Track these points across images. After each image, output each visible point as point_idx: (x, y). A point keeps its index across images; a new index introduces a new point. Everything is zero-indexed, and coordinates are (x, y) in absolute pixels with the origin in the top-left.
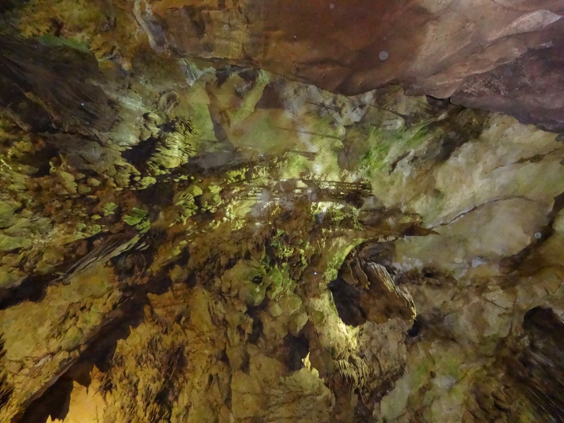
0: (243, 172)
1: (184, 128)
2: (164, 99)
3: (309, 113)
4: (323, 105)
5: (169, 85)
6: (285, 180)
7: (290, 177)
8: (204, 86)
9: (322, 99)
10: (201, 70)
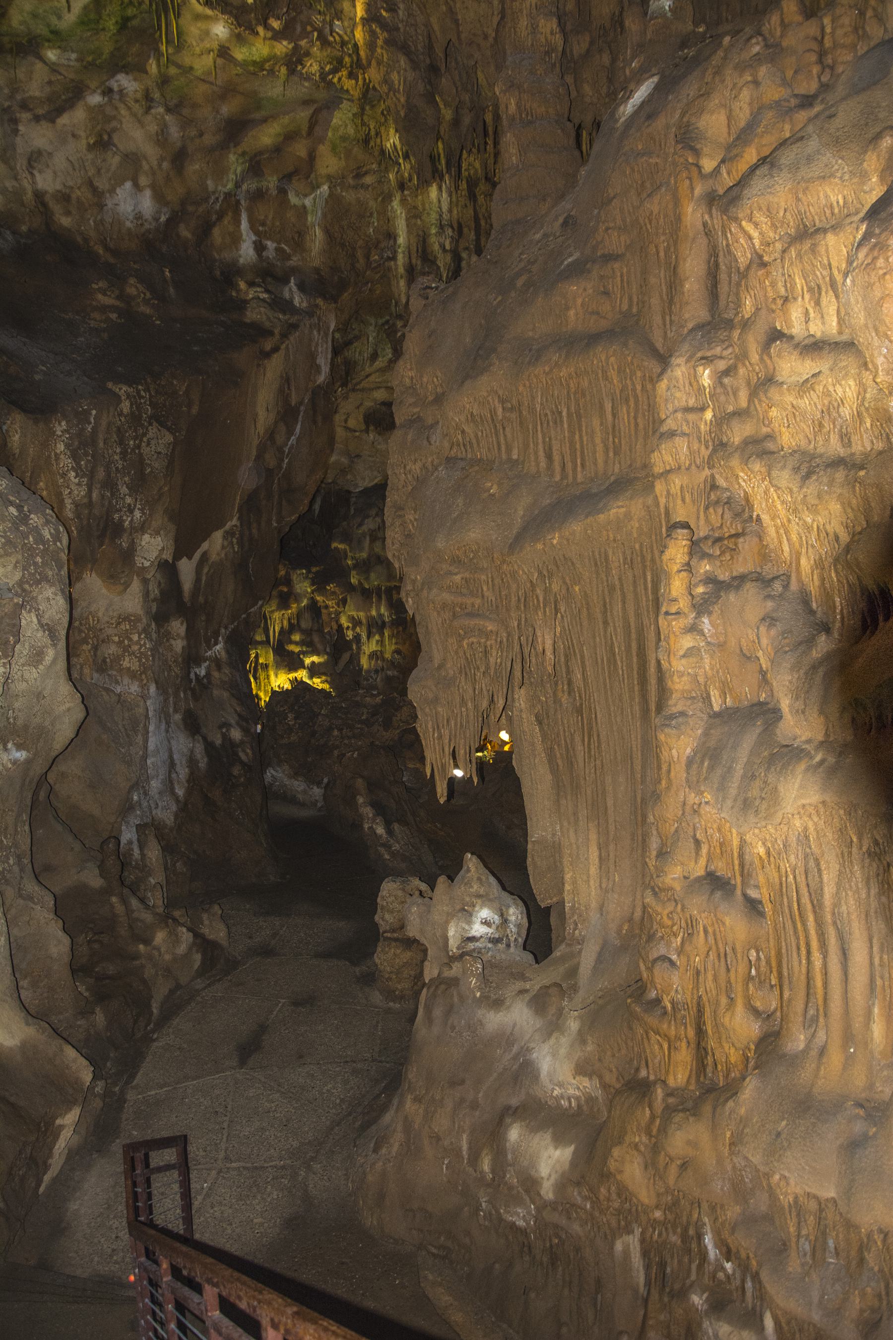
0: (340, 79)
1: (372, 143)
2: (368, 180)
3: (194, 106)
4: (168, 110)
5: (349, 196)
6: (285, 43)
7: (275, 43)
8: (313, 176)
9: (167, 117)
10: (304, 207)
